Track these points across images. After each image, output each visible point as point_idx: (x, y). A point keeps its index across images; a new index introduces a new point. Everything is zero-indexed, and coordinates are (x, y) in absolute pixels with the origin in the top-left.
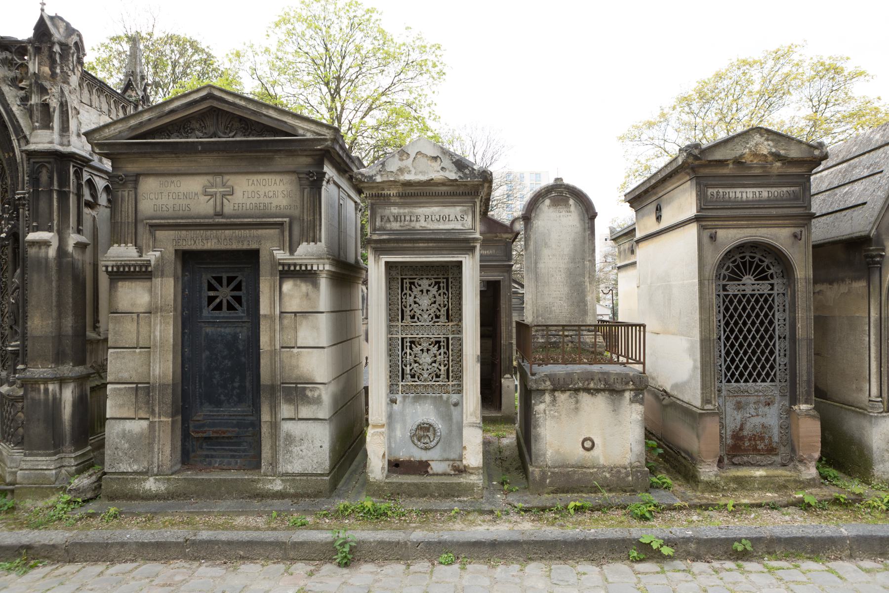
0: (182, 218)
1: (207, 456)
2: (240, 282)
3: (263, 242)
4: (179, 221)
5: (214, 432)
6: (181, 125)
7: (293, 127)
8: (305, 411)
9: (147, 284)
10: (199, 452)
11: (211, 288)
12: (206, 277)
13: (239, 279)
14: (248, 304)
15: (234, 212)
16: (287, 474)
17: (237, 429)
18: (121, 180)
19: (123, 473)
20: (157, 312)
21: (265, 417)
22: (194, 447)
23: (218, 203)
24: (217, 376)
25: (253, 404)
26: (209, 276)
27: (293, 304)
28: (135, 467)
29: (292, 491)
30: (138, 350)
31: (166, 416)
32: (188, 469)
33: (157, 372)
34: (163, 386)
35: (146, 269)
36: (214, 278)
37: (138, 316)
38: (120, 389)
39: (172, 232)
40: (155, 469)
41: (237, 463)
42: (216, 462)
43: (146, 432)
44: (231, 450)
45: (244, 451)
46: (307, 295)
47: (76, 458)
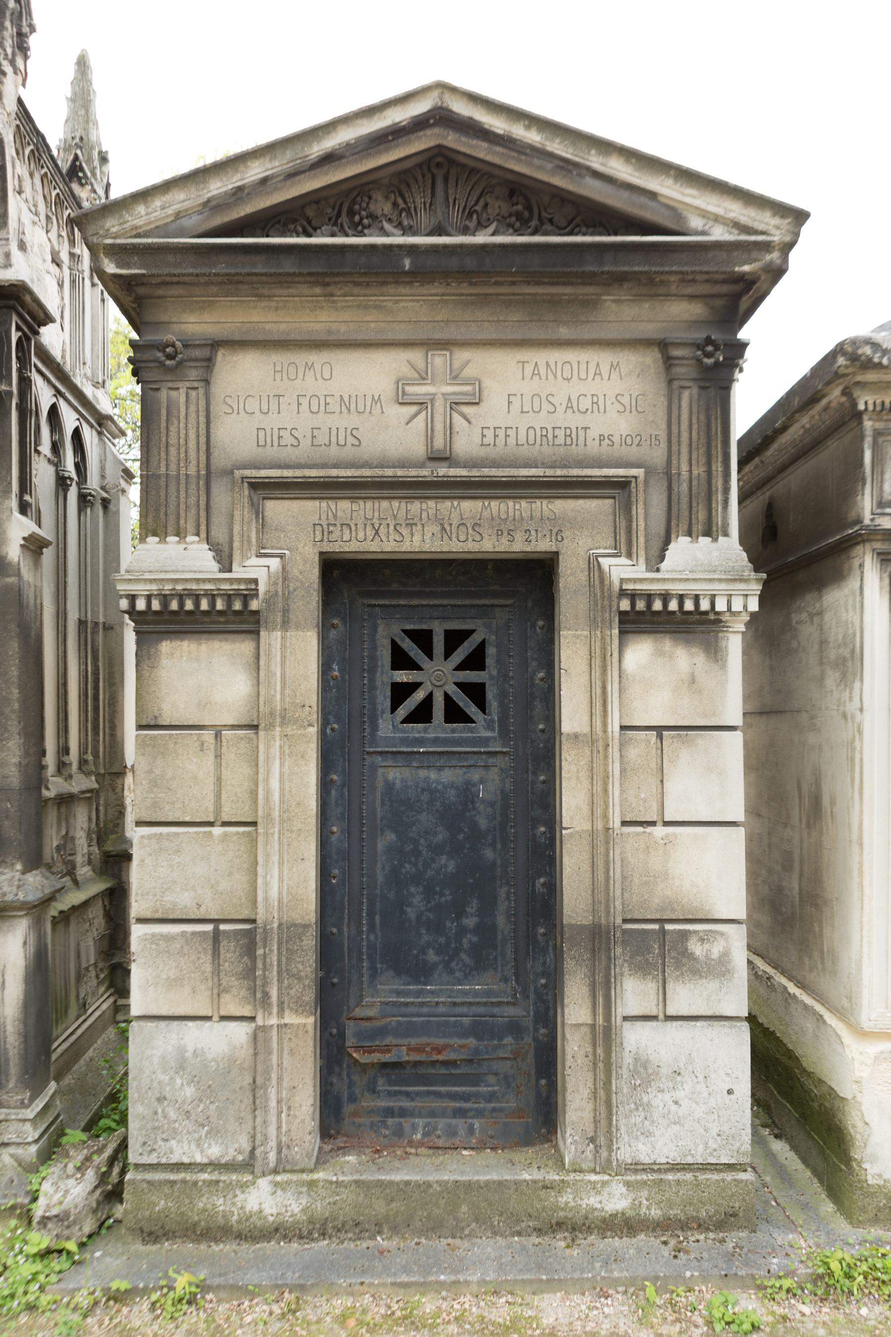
0: (336, 466)
1: (389, 1112)
2: (482, 645)
3: (567, 534)
4: (334, 472)
5: (410, 1049)
6: (345, 204)
7: (673, 210)
8: (685, 997)
9: (245, 647)
10: (368, 1102)
11: (401, 660)
12: (386, 632)
13: (476, 639)
14: (501, 705)
15: (483, 452)
16: (636, 1167)
17: (472, 1041)
18: (170, 357)
19: (179, 1167)
20: (271, 726)
21: (576, 1009)
22: (356, 1089)
23: (439, 427)
24: (416, 900)
25: (517, 975)
26: (396, 629)
27: (655, 708)
28: (214, 1151)
29: (656, 1213)
30: (217, 831)
31: (299, 1008)
32: (342, 1150)
33: (274, 893)
34: (290, 931)
35: (245, 604)
36: (411, 634)
37: (218, 736)
38: (169, 938)
39: (311, 506)
40: (272, 1157)
41: (471, 1130)
42: (414, 1128)
43: (245, 1054)
44: (453, 1097)
45: (491, 1097)
46: (693, 680)
47: (34, 1121)
